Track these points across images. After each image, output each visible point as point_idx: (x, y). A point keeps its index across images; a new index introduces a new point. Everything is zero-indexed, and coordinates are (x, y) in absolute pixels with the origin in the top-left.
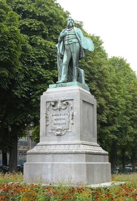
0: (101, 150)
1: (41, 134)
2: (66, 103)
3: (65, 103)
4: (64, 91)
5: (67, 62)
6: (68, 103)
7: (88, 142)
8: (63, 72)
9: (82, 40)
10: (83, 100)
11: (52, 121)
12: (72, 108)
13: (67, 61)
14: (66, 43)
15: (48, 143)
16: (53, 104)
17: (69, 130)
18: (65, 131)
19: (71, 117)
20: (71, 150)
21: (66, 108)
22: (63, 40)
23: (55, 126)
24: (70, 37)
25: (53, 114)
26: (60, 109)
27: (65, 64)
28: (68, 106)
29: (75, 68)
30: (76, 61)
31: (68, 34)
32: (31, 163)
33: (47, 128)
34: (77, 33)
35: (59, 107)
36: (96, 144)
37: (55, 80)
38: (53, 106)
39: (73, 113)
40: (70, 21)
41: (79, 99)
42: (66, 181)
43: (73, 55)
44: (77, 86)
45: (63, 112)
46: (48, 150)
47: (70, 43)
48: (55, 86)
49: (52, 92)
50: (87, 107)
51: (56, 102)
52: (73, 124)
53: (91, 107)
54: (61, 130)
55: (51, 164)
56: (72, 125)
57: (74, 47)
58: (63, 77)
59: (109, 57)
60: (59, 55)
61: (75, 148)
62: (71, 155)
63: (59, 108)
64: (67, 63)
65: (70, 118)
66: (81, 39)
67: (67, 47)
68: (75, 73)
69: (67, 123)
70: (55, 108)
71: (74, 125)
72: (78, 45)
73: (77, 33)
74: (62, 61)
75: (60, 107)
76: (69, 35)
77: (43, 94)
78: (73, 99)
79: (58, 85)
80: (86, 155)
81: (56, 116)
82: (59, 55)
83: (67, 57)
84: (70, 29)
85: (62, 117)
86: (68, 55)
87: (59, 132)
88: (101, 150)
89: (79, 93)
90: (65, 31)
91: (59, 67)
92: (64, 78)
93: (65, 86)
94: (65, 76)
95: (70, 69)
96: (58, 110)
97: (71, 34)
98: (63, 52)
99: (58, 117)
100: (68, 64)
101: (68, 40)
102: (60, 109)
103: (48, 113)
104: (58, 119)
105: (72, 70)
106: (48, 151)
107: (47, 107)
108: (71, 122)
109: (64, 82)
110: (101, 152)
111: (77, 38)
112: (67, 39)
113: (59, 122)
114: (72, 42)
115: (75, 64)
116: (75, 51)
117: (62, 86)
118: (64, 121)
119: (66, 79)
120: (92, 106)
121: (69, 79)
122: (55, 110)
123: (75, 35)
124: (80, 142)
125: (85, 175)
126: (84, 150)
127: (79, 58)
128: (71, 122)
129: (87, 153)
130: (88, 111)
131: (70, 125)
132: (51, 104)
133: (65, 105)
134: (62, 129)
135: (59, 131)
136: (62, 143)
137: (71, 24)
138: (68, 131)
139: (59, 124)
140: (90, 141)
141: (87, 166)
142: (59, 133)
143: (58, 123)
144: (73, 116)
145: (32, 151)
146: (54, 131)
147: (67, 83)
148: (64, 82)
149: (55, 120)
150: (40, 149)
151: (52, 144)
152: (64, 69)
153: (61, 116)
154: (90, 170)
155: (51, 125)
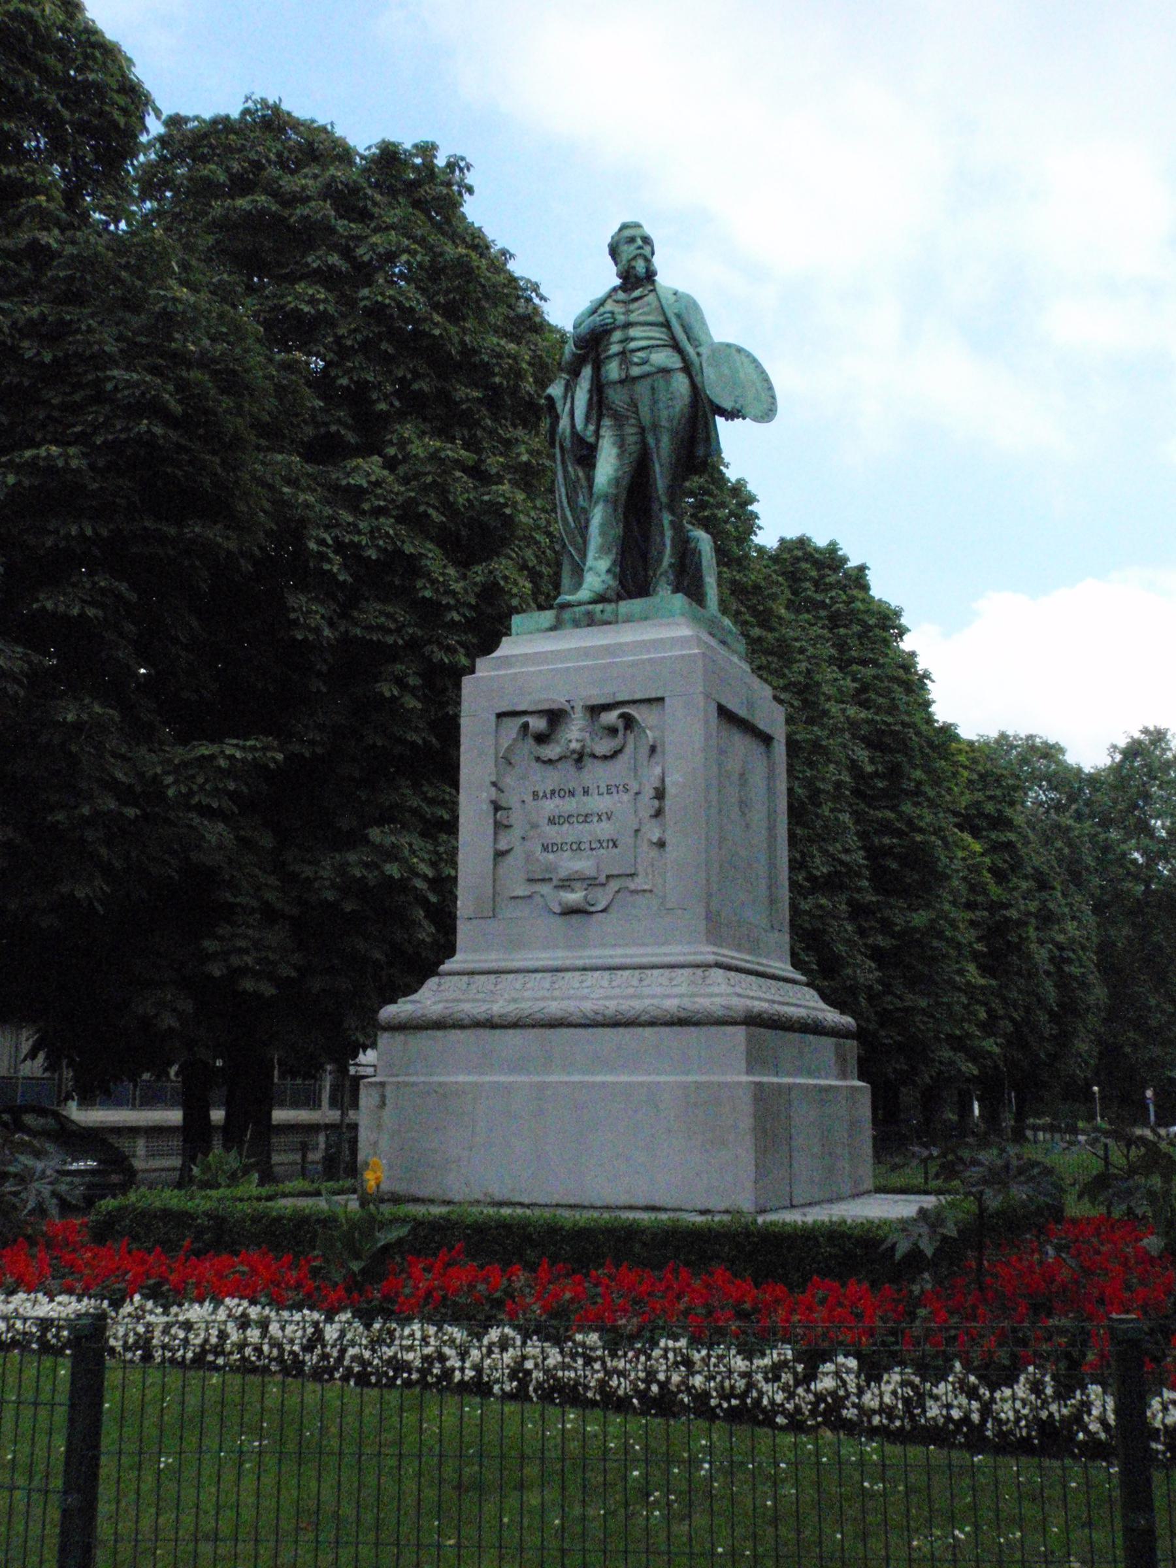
0: (806, 1003)
1: (465, 905)
2: (620, 720)
3: (611, 717)
4: (608, 650)
5: (617, 482)
6: (629, 722)
7: (748, 958)
8: (595, 538)
9: (704, 357)
10: (723, 702)
11: (534, 826)
12: (653, 749)
14: (613, 370)
15: (497, 963)
16: (538, 724)
17: (639, 883)
18: (614, 885)
19: (647, 803)
20: (655, 1001)
22: (592, 355)
23: (551, 856)
24: (633, 339)
25: (540, 789)
26: (579, 758)
28: (631, 738)
29: (666, 523)
31: (621, 318)
35: (574, 745)
36: (784, 967)
37: (545, 594)
39: (663, 781)
41: (701, 697)
42: (827, 1219)
43: (651, 441)
44: (682, 620)
45: (597, 774)
47: (635, 371)
48: (547, 625)
49: (535, 659)
50: (741, 744)
52: (661, 844)
53: (756, 748)
54: (591, 882)
56: (654, 853)
57: (663, 396)
58: (598, 571)
59: (767, 538)
60: (568, 444)
61: (676, 990)
63: (574, 752)
65: (646, 812)
66: (698, 354)
67: (617, 397)
68: (661, 553)
69: (626, 840)
70: (551, 751)
71: (671, 852)
72: (681, 383)
74: (584, 482)
75: (583, 747)
76: (628, 325)
77: (473, 672)
78: (662, 699)
79: (567, 615)
81: (557, 800)
82: (568, 444)
83: (620, 456)
84: (637, 293)
85: (598, 803)
86: (621, 444)
87: (573, 891)
88: (812, 1004)
89: (700, 663)
92: (604, 577)
93: (609, 623)
94: (604, 564)
96: (568, 766)
97: (642, 319)
98: (592, 428)
99: (569, 805)
100: (623, 497)
102: (579, 758)
103: (509, 781)
104: (568, 819)
105: (646, 537)
107: (505, 744)
109: (601, 599)
110: (820, 1016)
112: (615, 349)
113: (569, 833)
114: (647, 368)
115: (664, 499)
116: (664, 423)
117: (591, 621)
118: (604, 830)
119: (613, 583)
120: (762, 749)
121: (633, 580)
122: (550, 761)
123: (667, 325)
124: (707, 952)
125: (742, 1154)
129: (753, 1021)
130: (742, 775)
131: (647, 853)
132: (525, 726)
134: (593, 873)
135: (578, 885)
136: (599, 962)
138: (632, 886)
139: (577, 847)
140: (754, 947)
142: (574, 897)
143: (570, 839)
146: (545, 889)
147: (625, 607)
149: (552, 821)
152: (602, 525)
153: (585, 799)
154: (770, 1112)
155: (529, 857)
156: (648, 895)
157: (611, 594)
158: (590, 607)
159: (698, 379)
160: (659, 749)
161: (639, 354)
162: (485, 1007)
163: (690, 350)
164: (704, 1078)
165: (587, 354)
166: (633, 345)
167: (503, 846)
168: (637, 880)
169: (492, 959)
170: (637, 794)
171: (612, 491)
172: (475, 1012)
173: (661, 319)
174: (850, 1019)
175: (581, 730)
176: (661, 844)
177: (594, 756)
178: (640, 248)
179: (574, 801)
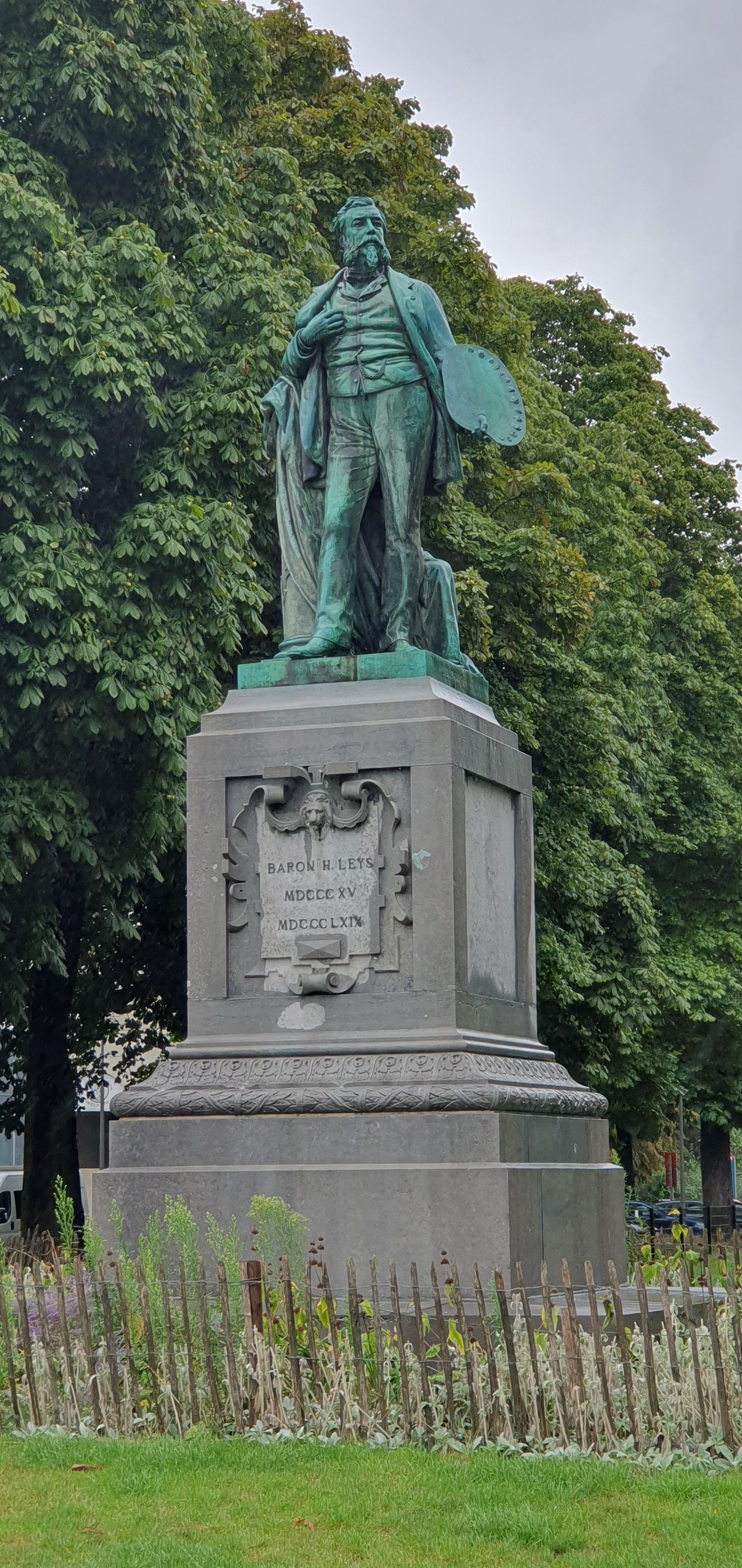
0: (552, 1082)
3: (353, 788)
5: (347, 514)
6: (372, 791)
9: (444, 367)
10: (471, 769)
12: (398, 823)
13: (348, 510)
21: (359, 825)
27: (339, 532)
30: (405, 509)
31: (352, 321)
32: (153, 1170)
33: (232, 953)
34: (414, 316)
36: (533, 1045)
38: (275, 807)
39: (409, 855)
40: (364, 230)
46: (256, 1087)
48: (275, 677)
51: (295, 785)
52: (408, 923)
55: (278, 1173)
56: (401, 931)
58: (314, 615)
62: (405, 1114)
64: (350, 520)
66: (437, 361)
68: (397, 595)
70: (288, 821)
73: (414, 316)
76: (359, 328)
78: (408, 769)
80: (502, 1121)
81: (295, 874)
83: (352, 482)
84: (368, 289)
88: (563, 1083)
90: (328, 297)
91: (288, 544)
93: (347, 679)
94: (337, 608)
95: (367, 562)
98: (319, 445)
99: (310, 880)
101: (355, 363)
106: (255, 1093)
107: (237, 811)
108: (398, 910)
109: (333, 650)
110: (570, 1095)
111: (413, 355)
112: (345, 357)
114: (381, 383)
120: (508, 802)
122: (287, 832)
123: (401, 328)
126: (487, 1088)
127: (428, 487)
128: (398, 910)
129: (509, 1107)
131: (393, 934)
132: (259, 793)
133: (359, 801)
137: (371, 255)
141: (512, 1187)
144: (406, 871)
145: (144, 1095)
147: (364, 661)
148: (333, 650)
149: (289, 896)
150: (194, 1081)
151: (271, 1049)
153: (325, 872)
156: (394, 975)
157: (346, 643)
158: (326, 660)
159: (438, 392)
160: (404, 820)
161: (372, 366)
162: (226, 1094)
163: (428, 358)
164: (455, 1166)
165: (312, 360)
166: (367, 354)
167: (236, 923)
168: (381, 959)
169: (231, 1041)
170: (381, 869)
171: (346, 523)
172: (215, 1099)
173: (395, 320)
174: (601, 1097)
175: (321, 800)
176: (408, 923)
177: (333, 827)
178: (372, 233)
179: (313, 875)
